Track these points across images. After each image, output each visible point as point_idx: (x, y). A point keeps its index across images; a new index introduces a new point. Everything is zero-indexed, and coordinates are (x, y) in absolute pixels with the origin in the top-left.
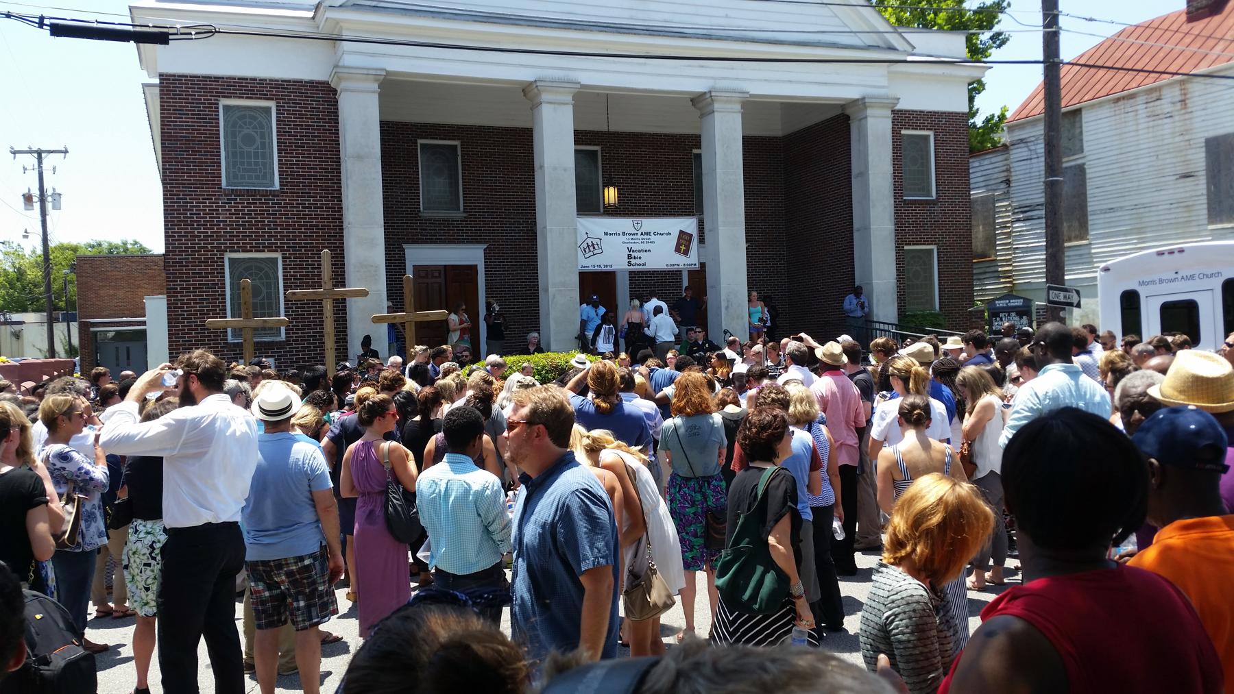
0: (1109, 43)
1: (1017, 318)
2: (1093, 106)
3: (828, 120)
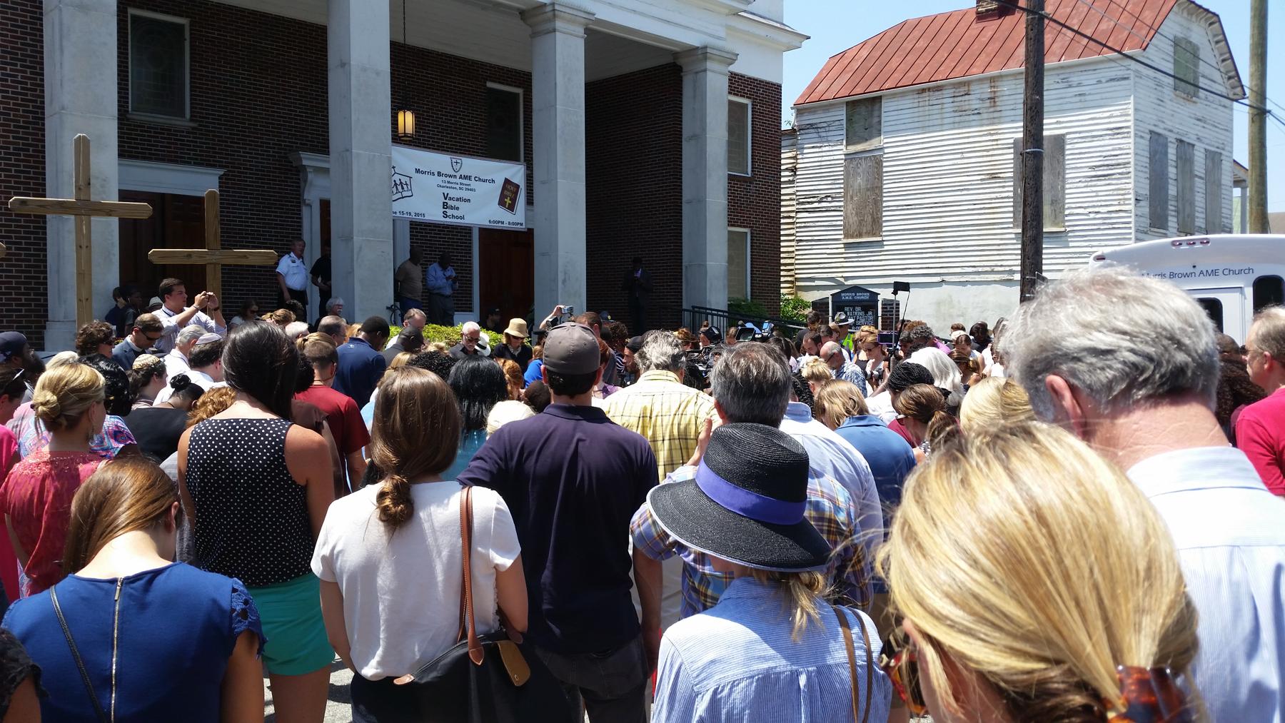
0: (893, 33)
1: (862, 313)
2: (894, 95)
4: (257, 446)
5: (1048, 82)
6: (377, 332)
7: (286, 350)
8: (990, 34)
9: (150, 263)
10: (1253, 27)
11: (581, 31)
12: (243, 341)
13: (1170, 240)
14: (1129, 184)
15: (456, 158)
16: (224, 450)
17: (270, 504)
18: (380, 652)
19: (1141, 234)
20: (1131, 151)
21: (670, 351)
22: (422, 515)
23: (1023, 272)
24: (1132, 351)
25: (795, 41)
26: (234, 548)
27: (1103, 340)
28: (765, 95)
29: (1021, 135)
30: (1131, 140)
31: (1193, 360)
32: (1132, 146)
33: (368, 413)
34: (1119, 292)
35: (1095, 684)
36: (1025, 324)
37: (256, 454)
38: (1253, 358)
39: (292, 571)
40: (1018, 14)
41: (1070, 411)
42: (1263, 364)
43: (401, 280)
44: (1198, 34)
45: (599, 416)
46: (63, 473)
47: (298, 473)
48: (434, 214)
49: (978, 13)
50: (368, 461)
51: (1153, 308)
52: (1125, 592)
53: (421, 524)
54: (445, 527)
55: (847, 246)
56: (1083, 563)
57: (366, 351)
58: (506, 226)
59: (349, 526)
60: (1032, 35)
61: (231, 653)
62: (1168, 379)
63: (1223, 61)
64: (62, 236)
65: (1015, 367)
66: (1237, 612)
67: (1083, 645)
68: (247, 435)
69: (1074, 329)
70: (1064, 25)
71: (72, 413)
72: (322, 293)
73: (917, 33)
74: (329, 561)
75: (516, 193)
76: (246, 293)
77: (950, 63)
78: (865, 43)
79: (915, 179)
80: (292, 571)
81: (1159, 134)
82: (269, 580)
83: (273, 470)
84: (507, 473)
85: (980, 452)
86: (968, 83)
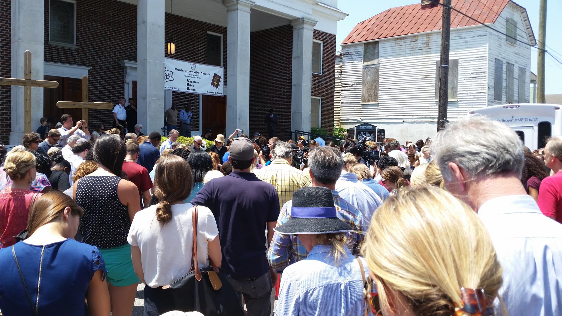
0: (385, 14)
2: (385, 41)
3: (278, 28)
4: (106, 188)
5: (452, 36)
6: (156, 139)
7: (120, 146)
8: (427, 15)
9: (57, 107)
10: (540, 14)
11: (249, 10)
12: (102, 142)
13: (502, 105)
14: (486, 81)
15: (193, 64)
16: (91, 190)
17: (111, 213)
18: (157, 276)
19: (490, 102)
20: (487, 67)
21: (285, 150)
22: (176, 218)
23: (439, 118)
24: (487, 153)
25: (342, 16)
26: (95, 232)
27: (475, 148)
28: (329, 40)
29: (439, 59)
30: (487, 62)
31: (513, 158)
32: (487, 65)
33: (152, 175)
34: (482, 128)
35: (450, 295)
36: (441, 140)
37: (105, 191)
38: (547, 157)
39: (121, 242)
40: (439, 7)
41: (459, 178)
42: (551, 160)
43: (167, 115)
44: (517, 17)
45: (253, 177)
46: (17, 197)
47: (124, 201)
48: (183, 88)
49: (422, 6)
50: (152, 195)
51: (496, 135)
52: (466, 256)
53: (175, 221)
54: (185, 223)
55: (363, 105)
56: (446, 243)
57: (151, 147)
58: (214, 94)
59: (144, 223)
60: (445, 15)
61: (91, 278)
62: (502, 166)
63: (527, 29)
64: (18, 95)
65: (434, 158)
66: (527, 265)
67: (445, 278)
68: (101, 183)
69: (463, 143)
70: (459, 12)
71: (22, 172)
72: (130, 123)
73: (395, 14)
74: (135, 238)
75: (219, 80)
76: (98, 122)
77: (409, 27)
78: (372, 18)
79: (393, 77)
80: (121, 242)
81: (499, 60)
82: (111, 246)
83: (112, 199)
84: (211, 201)
85: (403, 196)
86: (417, 36)
